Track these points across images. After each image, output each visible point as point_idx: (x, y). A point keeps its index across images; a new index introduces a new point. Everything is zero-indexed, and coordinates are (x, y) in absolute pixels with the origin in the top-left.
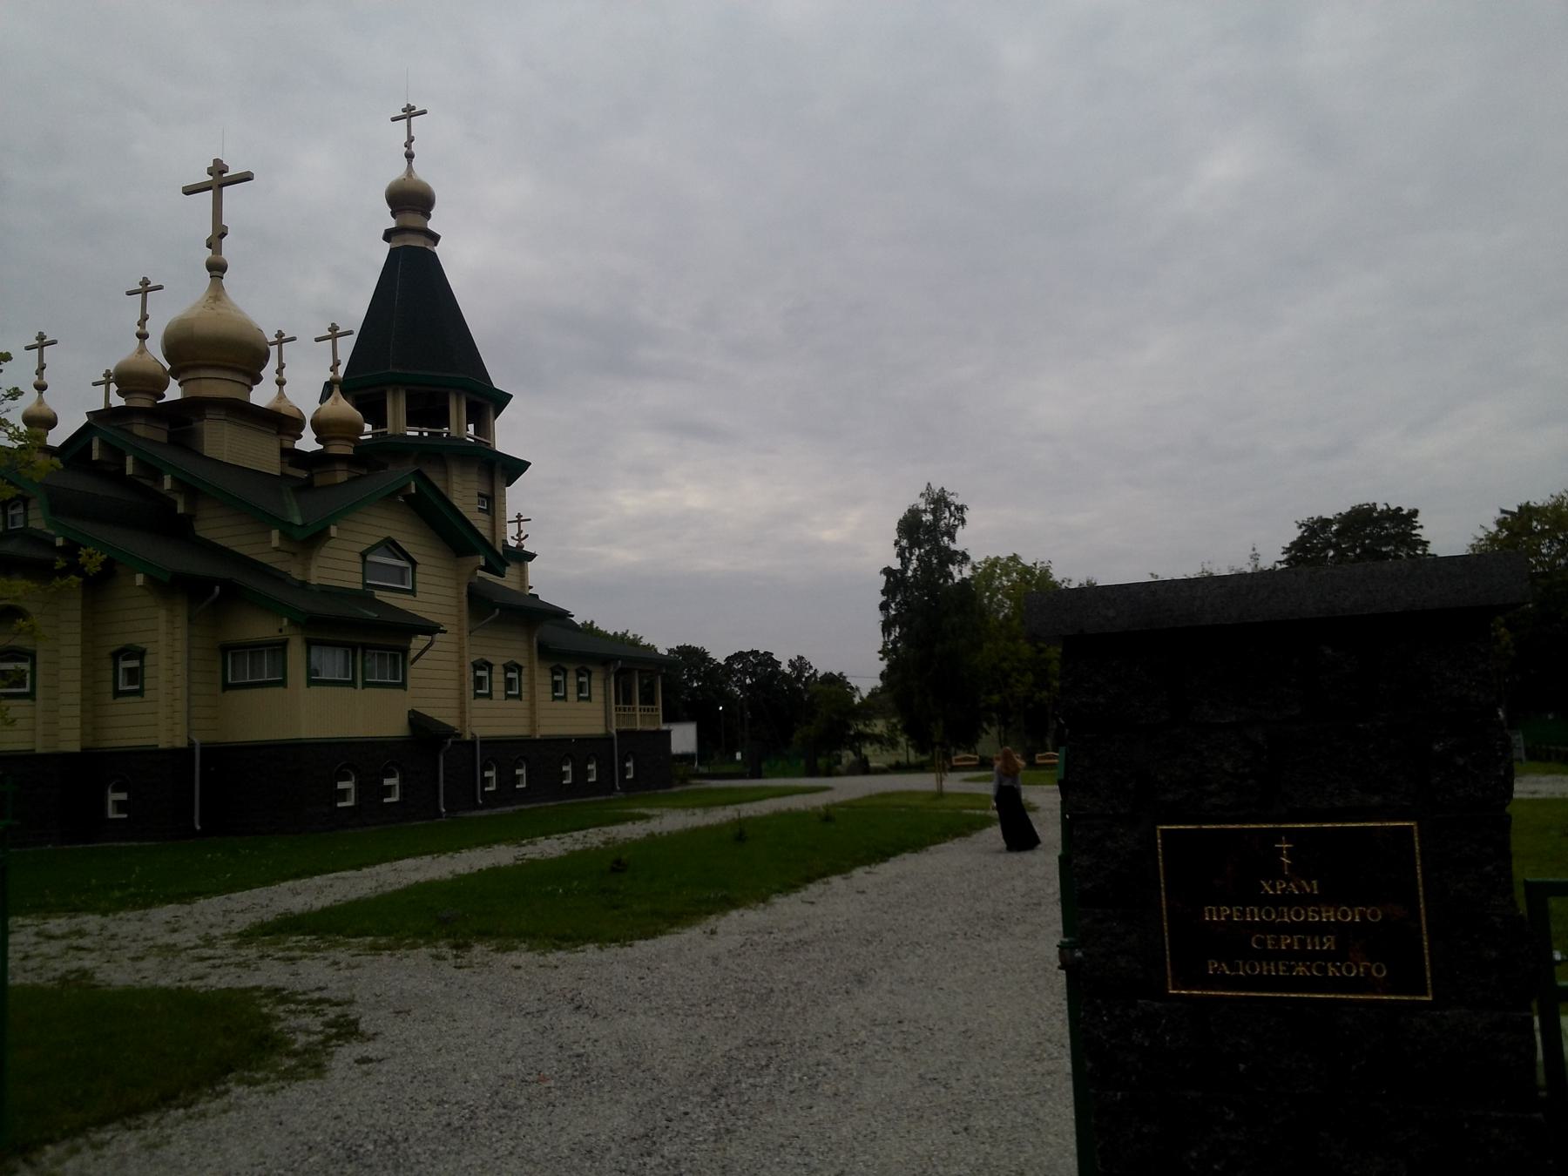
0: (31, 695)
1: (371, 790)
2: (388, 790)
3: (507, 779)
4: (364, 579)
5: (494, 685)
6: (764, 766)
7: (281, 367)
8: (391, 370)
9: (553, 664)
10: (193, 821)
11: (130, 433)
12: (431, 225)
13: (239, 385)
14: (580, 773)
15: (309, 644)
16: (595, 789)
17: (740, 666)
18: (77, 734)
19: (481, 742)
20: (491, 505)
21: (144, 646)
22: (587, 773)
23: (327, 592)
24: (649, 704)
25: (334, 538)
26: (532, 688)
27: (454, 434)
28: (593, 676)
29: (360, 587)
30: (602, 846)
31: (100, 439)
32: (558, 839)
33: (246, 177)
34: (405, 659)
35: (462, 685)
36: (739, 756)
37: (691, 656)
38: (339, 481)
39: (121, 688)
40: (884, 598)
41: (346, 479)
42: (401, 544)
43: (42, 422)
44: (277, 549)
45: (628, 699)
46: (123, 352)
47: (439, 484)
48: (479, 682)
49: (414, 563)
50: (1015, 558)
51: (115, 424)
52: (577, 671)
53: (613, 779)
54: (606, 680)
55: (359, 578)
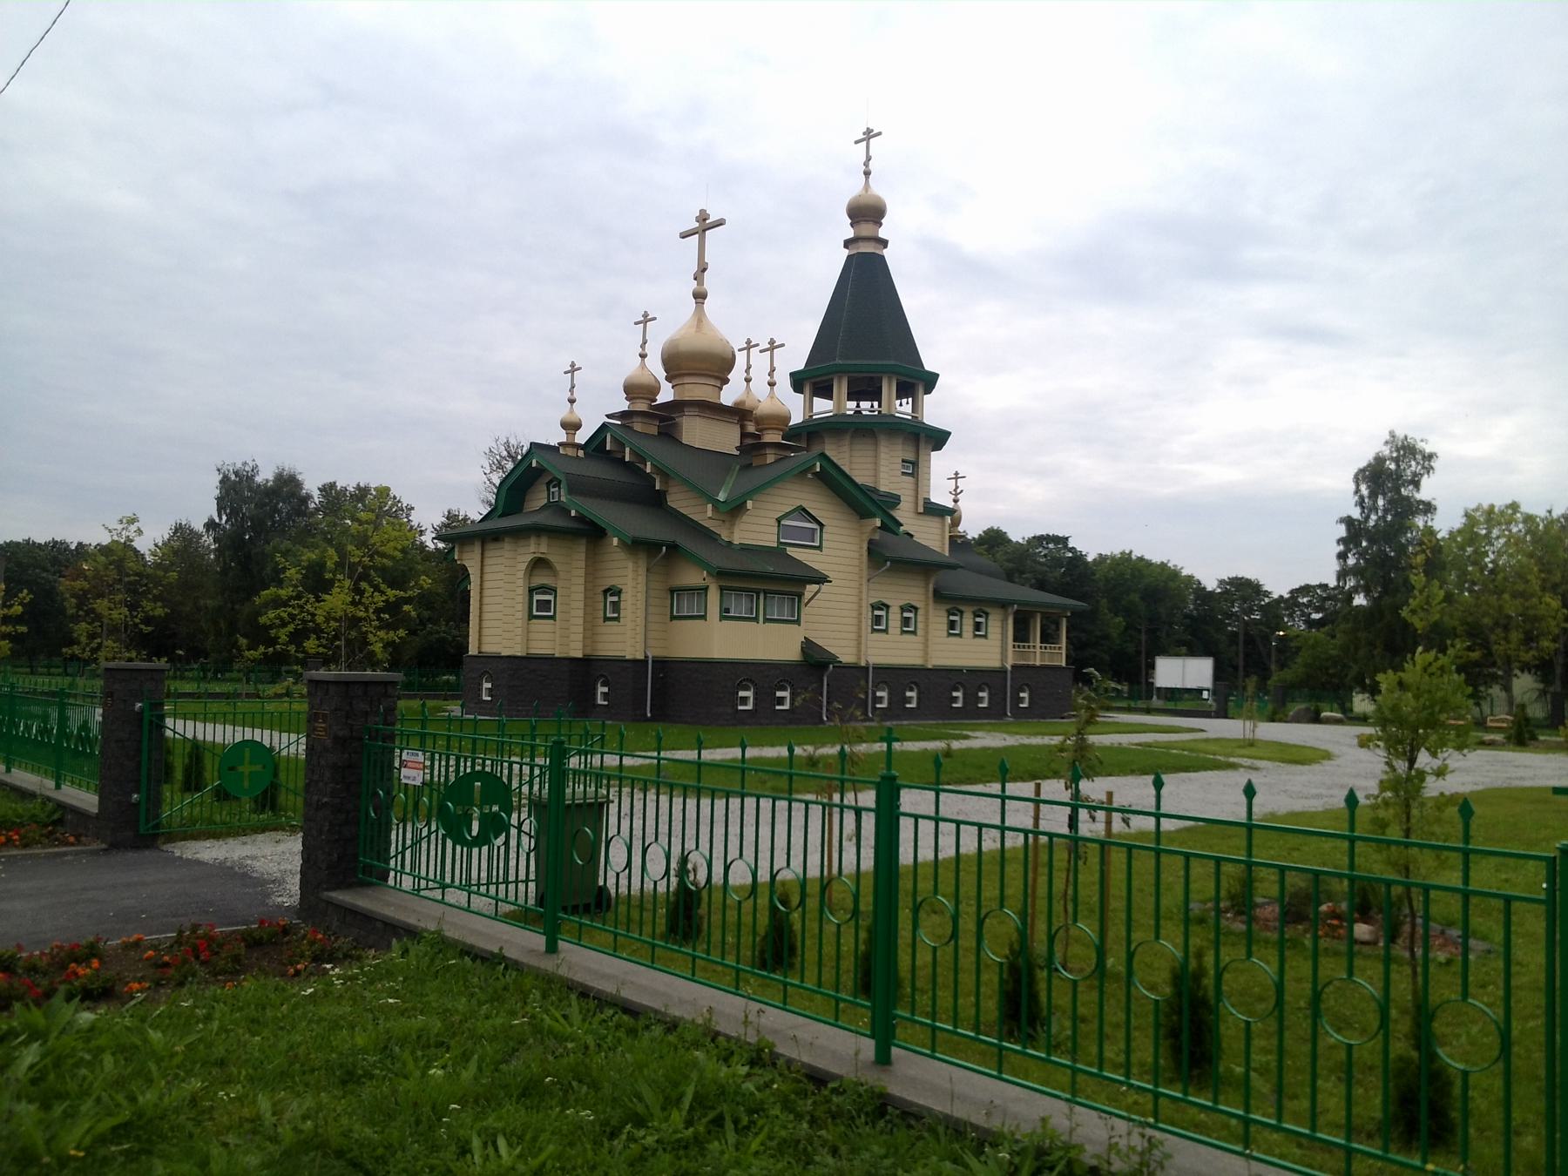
0: (552, 618)
2: (909, 700)
4: (778, 539)
10: (646, 710)
15: (722, 589)
16: (984, 714)
18: (580, 645)
23: (747, 549)
27: (884, 411)
28: (990, 617)
29: (775, 545)
34: (799, 602)
37: (1243, 590)
39: (608, 615)
40: (1342, 548)
44: (710, 518)
46: (630, 367)
48: (877, 620)
50: (1514, 506)
54: (1004, 620)
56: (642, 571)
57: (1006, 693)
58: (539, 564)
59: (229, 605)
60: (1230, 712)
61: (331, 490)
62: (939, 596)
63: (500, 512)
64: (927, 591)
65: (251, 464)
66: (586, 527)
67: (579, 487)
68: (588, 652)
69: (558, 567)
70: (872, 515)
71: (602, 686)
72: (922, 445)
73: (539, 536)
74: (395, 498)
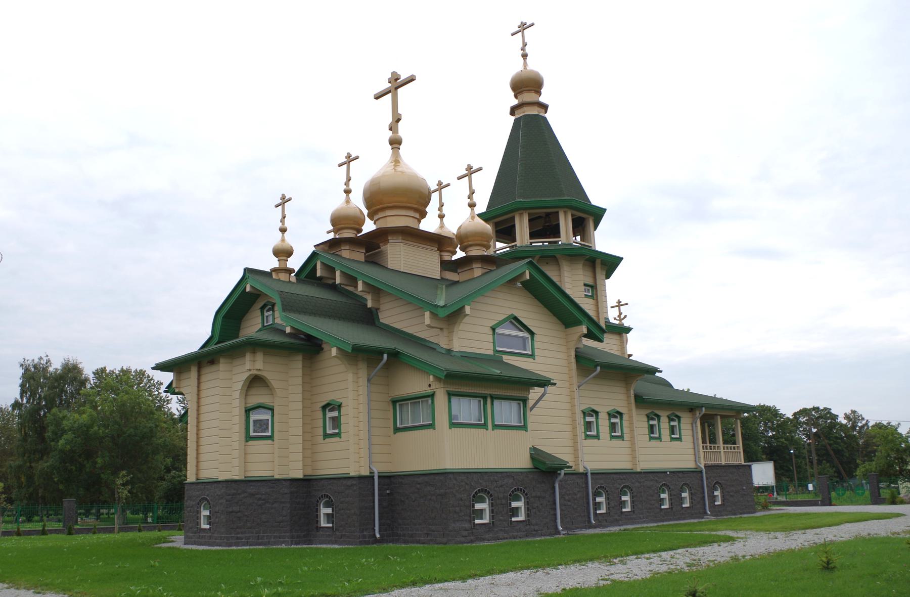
0: (270, 438)
1: (503, 511)
3: (616, 505)
5: (600, 428)
6: (833, 494)
7: (442, 205)
8: (517, 200)
9: (648, 411)
11: (340, 256)
12: (542, 99)
13: (411, 218)
14: (676, 499)
15: (450, 395)
17: (804, 419)
19: (592, 474)
20: (594, 292)
21: (340, 401)
22: (682, 500)
24: (733, 444)
25: (468, 315)
26: (632, 430)
28: (682, 420)
29: (491, 353)
30: (686, 569)
31: (321, 262)
32: (648, 559)
33: (480, 169)
35: (575, 428)
36: (810, 487)
38: (475, 277)
39: (328, 432)
41: (480, 274)
42: (529, 327)
43: (283, 253)
44: (429, 326)
45: (713, 440)
46: (335, 202)
47: (555, 279)
48: (588, 426)
49: (532, 333)
51: (332, 252)
52: (668, 417)
53: (704, 504)
54: (693, 424)
55: (491, 346)
56: (363, 381)
57: (703, 493)
58: (256, 381)
59: (28, 464)
60: (834, 502)
61: (102, 373)
62: (640, 401)
63: (216, 339)
64: (629, 397)
65: (45, 359)
66: (303, 342)
67: (291, 305)
68: (309, 472)
69: (274, 384)
70: (578, 323)
71: (324, 507)
72: (598, 270)
73: (254, 352)
74: (149, 376)
